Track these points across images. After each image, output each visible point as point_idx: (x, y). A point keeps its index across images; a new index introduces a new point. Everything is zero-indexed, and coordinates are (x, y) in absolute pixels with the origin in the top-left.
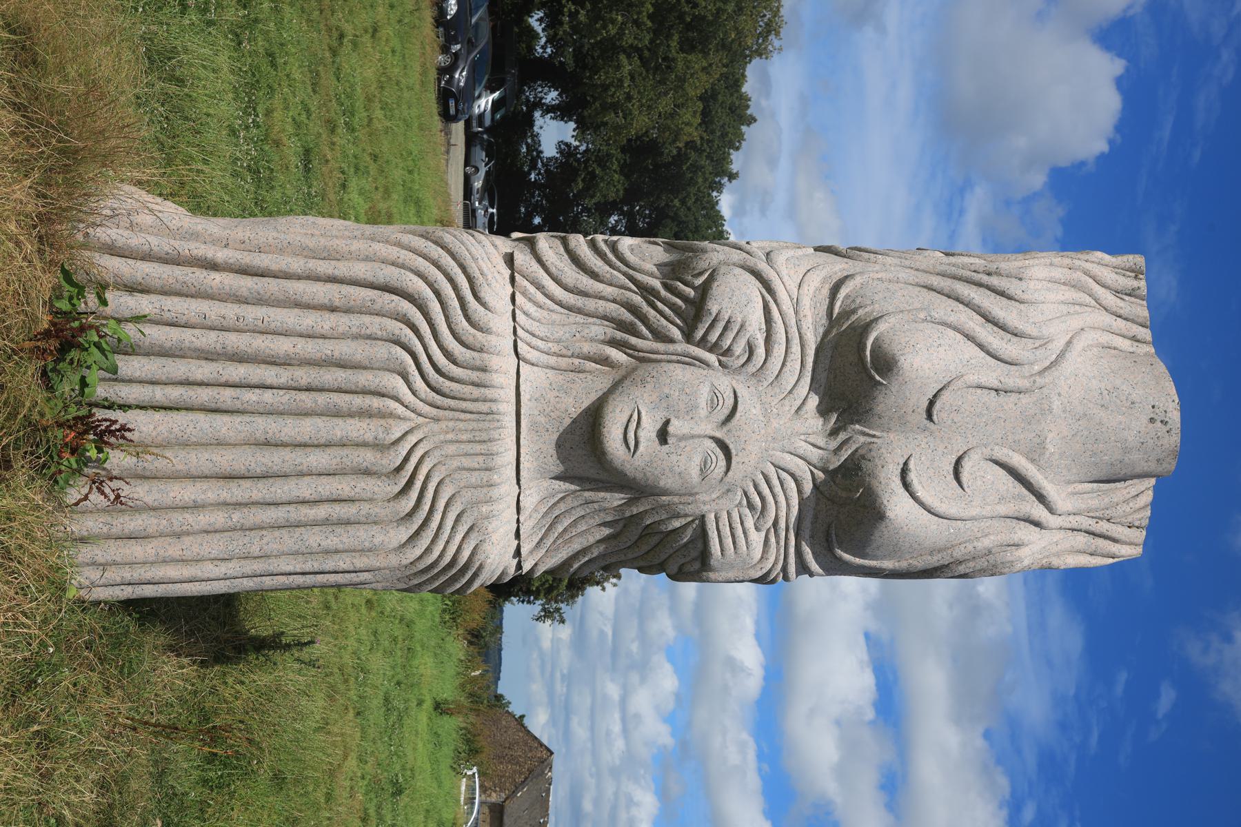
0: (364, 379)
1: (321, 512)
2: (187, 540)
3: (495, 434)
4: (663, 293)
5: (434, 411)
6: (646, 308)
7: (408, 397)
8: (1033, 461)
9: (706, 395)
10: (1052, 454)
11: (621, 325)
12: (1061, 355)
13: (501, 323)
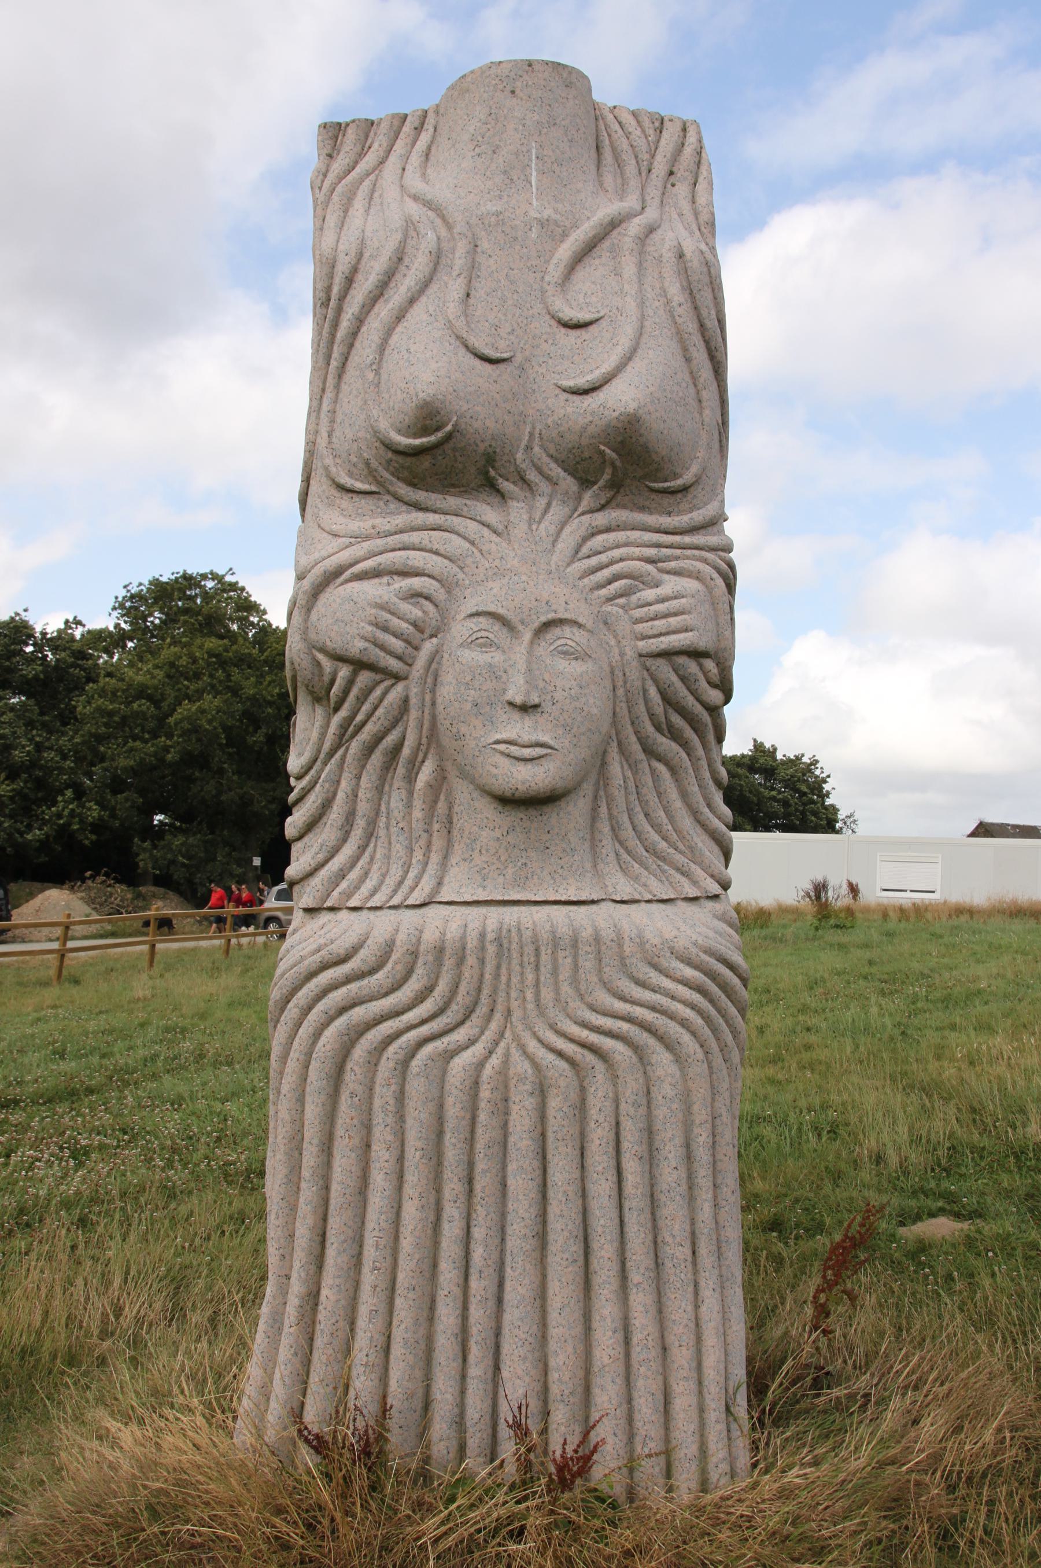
0: (454, 1109)
1: (632, 1167)
2: (671, 1339)
3: (527, 934)
4: (343, 713)
5: (498, 1016)
6: (365, 735)
7: (477, 1050)
8: (565, 235)
9: (474, 654)
10: (556, 211)
12: (428, 204)
13: (382, 926)
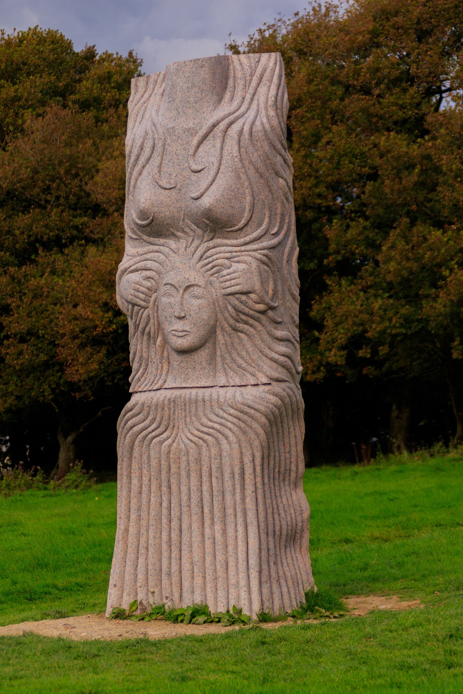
2: (262, 547)
8: (197, 133)
10: (194, 124)
11: (149, 339)
